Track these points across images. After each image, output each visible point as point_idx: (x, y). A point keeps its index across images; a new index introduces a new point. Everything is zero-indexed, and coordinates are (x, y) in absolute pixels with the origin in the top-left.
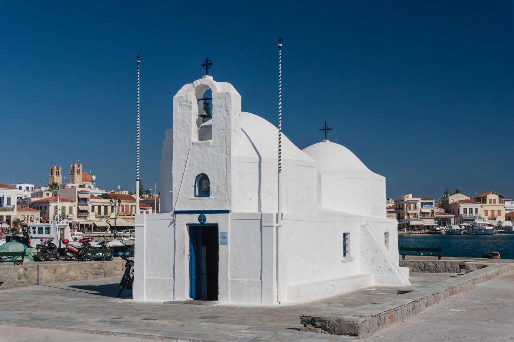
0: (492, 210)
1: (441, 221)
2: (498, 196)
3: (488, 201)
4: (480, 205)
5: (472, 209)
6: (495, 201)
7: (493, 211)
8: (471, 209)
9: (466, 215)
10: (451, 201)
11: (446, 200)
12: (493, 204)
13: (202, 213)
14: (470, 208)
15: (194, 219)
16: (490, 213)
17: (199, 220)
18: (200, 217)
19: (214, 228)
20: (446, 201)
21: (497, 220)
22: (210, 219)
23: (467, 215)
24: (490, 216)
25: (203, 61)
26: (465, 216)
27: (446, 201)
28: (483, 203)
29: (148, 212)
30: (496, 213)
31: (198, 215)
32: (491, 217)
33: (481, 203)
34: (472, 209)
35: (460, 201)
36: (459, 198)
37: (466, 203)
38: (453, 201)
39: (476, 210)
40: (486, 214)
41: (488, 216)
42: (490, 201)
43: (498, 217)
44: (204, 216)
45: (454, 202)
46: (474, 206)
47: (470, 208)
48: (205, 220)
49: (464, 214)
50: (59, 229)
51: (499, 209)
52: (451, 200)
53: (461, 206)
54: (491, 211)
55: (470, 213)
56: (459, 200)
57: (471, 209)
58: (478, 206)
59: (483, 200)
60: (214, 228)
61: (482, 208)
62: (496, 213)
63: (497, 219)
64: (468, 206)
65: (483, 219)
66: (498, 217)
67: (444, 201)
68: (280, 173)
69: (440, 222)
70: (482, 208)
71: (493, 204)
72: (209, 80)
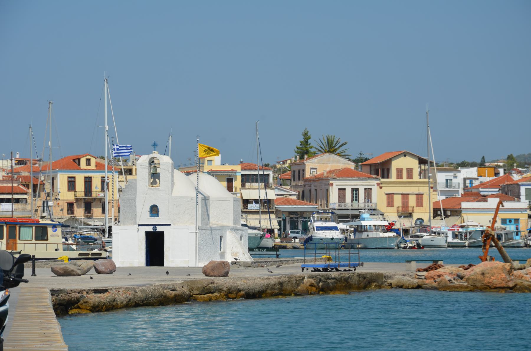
0: (404, 193)
1: (288, 219)
2: (417, 162)
3: (394, 172)
4: (378, 182)
5: (357, 190)
6: (410, 171)
7: (405, 196)
8: (355, 191)
9: (343, 204)
10: (312, 170)
11: (300, 168)
12: (405, 179)
13: (155, 226)
14: (353, 190)
15: (150, 229)
16: (398, 201)
17: (153, 229)
18: (153, 227)
19: (162, 234)
20: (299, 171)
21: (416, 216)
22: (159, 229)
23: (360, 205)
24: (398, 207)
25: (153, 143)
26: (343, 207)
27: (299, 171)
28: (383, 177)
29: (497, 235)
30: (412, 201)
31: (153, 227)
32: (400, 209)
33: (379, 177)
34: (357, 190)
35: (330, 172)
36: (330, 165)
37: (342, 177)
38: (315, 170)
39: (368, 192)
40: (390, 203)
41: (393, 206)
42: (399, 171)
43: (417, 209)
44: (156, 227)
45: (318, 173)
46: (362, 185)
47: (353, 190)
48: (156, 230)
49: (340, 204)
50: (315, 228)
51: (415, 190)
52: (311, 168)
53: (332, 185)
54: (400, 196)
55: (352, 201)
56: (328, 170)
57: (355, 191)
58: (372, 184)
59: (383, 171)
60: (162, 234)
61: (381, 188)
62: (412, 201)
63: (414, 214)
64: (349, 185)
65: (383, 215)
66: (417, 209)
67: (294, 171)
68: (197, 206)
69: (284, 221)
70: (381, 188)
71: (405, 179)
72: (156, 154)
